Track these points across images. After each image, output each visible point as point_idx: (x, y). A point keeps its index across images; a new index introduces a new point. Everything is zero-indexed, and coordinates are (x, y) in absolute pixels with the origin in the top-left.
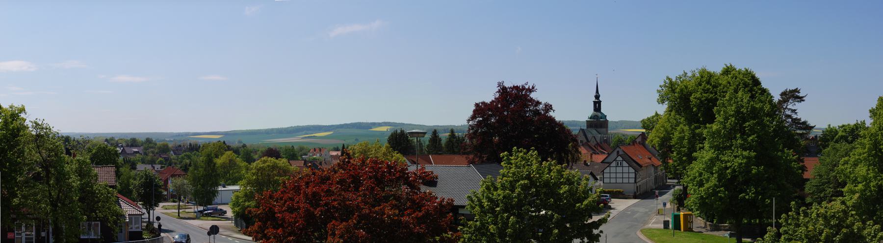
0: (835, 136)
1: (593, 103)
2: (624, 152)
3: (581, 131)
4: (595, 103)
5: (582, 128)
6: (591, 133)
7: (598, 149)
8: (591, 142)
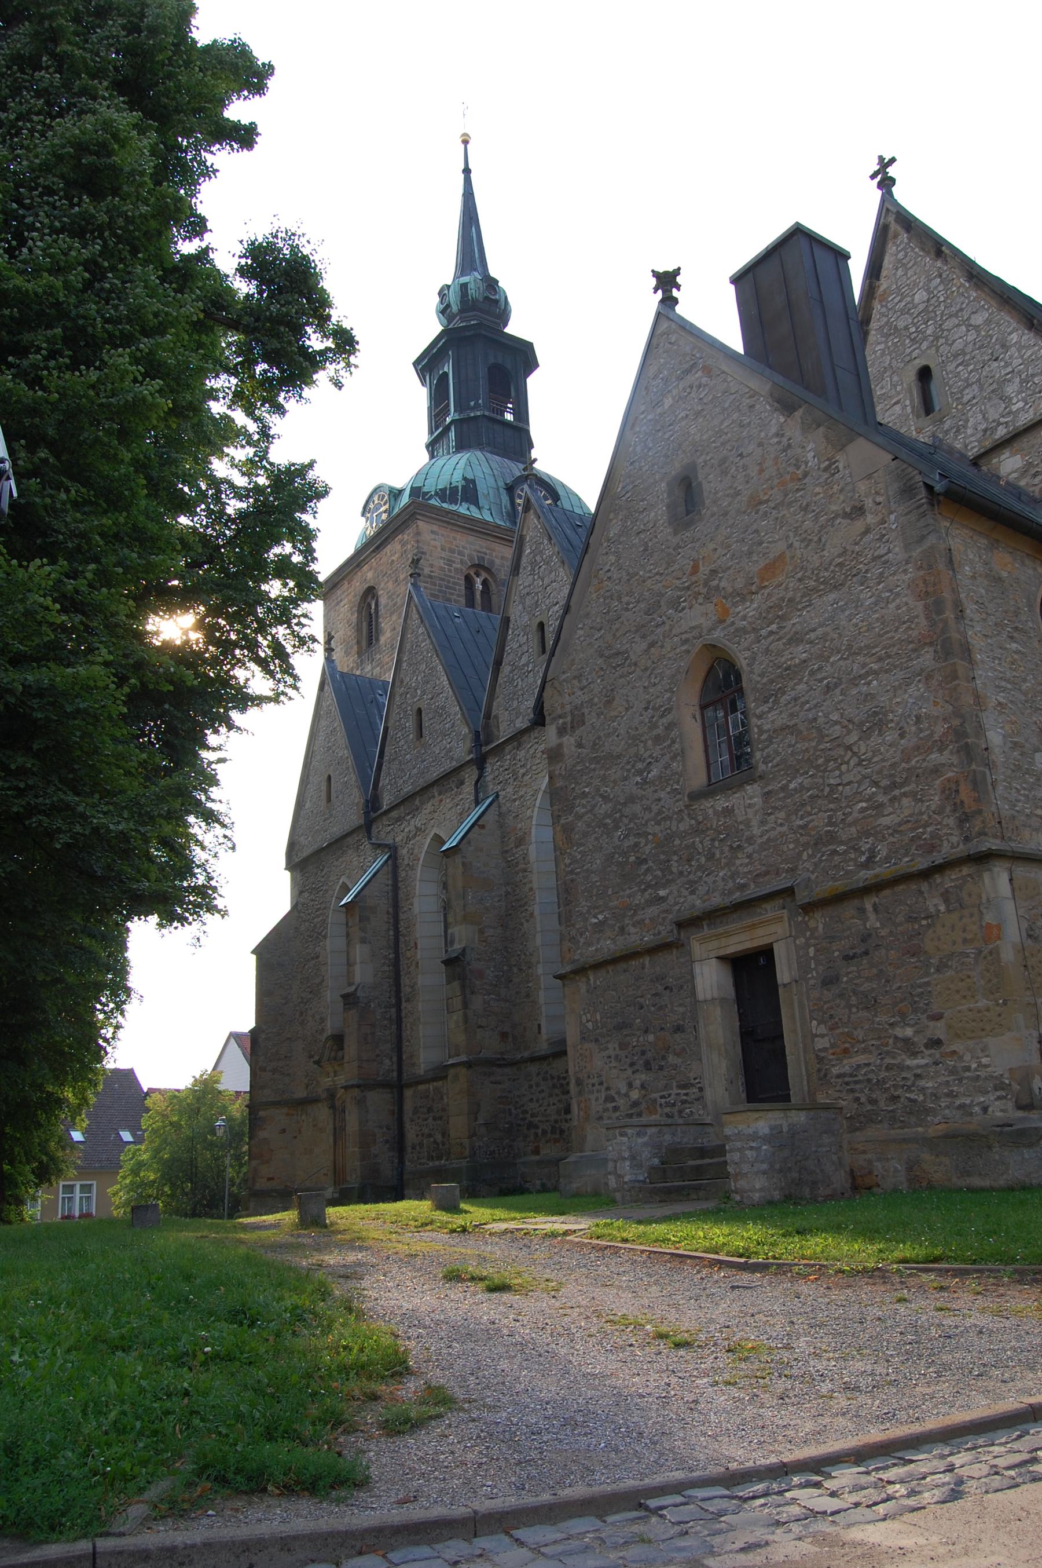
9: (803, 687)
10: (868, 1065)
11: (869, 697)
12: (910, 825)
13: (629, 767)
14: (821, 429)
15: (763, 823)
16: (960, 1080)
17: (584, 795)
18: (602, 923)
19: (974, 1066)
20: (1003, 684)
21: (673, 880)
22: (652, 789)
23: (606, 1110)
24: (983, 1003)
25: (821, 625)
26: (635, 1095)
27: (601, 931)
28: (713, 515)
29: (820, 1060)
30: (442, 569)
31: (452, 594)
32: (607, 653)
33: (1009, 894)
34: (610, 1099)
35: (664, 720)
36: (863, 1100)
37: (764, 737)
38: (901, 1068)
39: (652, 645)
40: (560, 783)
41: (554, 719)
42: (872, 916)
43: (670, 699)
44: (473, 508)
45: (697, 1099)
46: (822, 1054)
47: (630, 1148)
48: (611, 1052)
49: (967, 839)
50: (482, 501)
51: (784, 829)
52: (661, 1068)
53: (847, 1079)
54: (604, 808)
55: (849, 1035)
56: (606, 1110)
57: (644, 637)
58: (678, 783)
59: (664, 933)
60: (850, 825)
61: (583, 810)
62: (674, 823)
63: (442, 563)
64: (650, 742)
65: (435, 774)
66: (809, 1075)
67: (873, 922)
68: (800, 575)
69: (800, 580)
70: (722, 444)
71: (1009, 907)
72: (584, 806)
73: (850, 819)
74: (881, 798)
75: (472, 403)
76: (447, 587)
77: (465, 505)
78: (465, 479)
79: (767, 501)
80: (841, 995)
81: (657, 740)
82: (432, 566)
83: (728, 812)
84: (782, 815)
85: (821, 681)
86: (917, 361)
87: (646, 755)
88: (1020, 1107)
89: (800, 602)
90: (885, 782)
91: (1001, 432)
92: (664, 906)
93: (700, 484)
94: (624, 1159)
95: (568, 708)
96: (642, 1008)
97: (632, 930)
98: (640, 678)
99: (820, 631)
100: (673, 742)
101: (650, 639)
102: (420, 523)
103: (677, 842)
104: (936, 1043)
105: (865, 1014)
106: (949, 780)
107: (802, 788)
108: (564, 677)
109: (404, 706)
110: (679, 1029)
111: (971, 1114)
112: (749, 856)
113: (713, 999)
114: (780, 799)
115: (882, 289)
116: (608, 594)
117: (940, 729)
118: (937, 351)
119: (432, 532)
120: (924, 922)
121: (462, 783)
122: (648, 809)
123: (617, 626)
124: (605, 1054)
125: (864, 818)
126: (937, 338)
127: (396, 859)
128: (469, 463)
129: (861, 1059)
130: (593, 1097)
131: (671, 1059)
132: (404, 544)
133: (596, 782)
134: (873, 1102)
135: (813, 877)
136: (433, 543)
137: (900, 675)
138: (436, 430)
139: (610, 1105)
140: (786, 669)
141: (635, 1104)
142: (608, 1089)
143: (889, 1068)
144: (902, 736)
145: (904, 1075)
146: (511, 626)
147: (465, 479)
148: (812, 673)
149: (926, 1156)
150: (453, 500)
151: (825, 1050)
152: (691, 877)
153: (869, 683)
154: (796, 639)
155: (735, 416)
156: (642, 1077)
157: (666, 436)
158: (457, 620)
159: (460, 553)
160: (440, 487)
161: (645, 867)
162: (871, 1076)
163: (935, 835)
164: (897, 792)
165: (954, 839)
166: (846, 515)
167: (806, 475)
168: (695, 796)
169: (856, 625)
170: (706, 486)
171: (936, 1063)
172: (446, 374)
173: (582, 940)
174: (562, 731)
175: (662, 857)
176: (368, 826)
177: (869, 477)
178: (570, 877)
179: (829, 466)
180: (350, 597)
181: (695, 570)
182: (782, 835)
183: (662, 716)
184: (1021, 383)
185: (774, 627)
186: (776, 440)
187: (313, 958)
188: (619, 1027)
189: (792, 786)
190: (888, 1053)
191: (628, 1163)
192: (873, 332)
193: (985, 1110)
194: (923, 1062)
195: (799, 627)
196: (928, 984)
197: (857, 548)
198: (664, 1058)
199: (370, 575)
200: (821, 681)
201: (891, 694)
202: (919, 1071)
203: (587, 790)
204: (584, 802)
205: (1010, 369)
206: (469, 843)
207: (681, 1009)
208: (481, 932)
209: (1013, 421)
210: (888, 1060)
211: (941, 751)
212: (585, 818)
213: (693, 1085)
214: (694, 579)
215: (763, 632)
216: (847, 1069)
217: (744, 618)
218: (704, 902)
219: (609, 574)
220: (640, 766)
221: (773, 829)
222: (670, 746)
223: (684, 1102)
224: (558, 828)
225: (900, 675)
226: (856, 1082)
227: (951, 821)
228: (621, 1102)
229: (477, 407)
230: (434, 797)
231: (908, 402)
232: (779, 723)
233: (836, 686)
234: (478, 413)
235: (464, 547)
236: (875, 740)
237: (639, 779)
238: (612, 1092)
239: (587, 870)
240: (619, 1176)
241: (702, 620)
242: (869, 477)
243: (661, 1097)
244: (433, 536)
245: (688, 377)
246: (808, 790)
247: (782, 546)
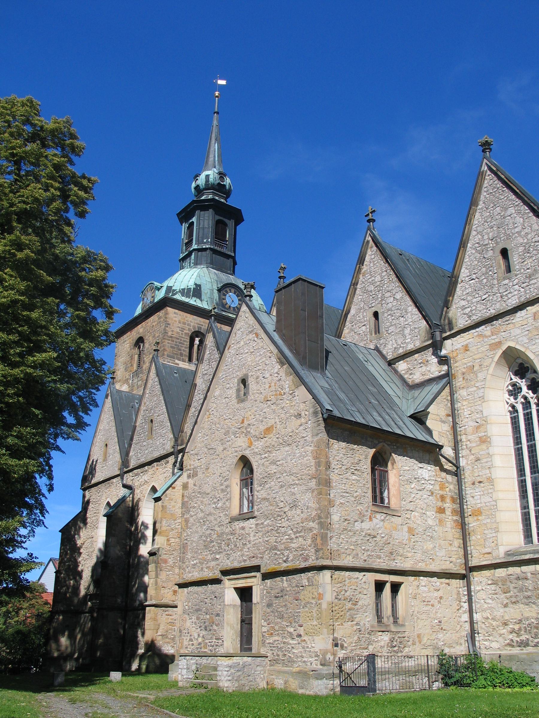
9: (273, 483)
10: (278, 640)
11: (294, 494)
12: (300, 549)
13: (211, 499)
14: (291, 376)
15: (255, 536)
16: (305, 651)
17: (194, 507)
18: (195, 565)
19: (310, 646)
20: (345, 494)
21: (221, 552)
22: (219, 511)
23: (189, 645)
24: (315, 623)
25: (282, 460)
26: (200, 640)
27: (194, 568)
28: (251, 400)
29: (263, 636)
30: (178, 333)
31: (182, 347)
32: (208, 447)
33: (330, 582)
34: (191, 640)
35: (225, 483)
36: (275, 654)
37: (258, 500)
38: (288, 644)
39: (225, 449)
40: (186, 499)
41: (187, 470)
42: (285, 582)
43: (228, 475)
44: (198, 300)
45: (221, 645)
46: (264, 634)
47: (187, 665)
48: (193, 620)
49: (317, 559)
50: (203, 297)
51: (261, 540)
52: (210, 630)
53: (271, 645)
54: (201, 515)
55: (273, 627)
56: (189, 645)
57: (222, 444)
58: (227, 511)
59: (216, 574)
60: (282, 544)
61: (193, 514)
62: (225, 528)
63: (178, 330)
64: (220, 491)
65: (156, 455)
66: (259, 641)
67: (285, 584)
68: (277, 436)
69: (277, 438)
70: (259, 370)
71: (329, 588)
72: (194, 512)
73: (282, 542)
74: (293, 536)
75: (205, 241)
76: (180, 343)
77: (194, 299)
78: (196, 284)
79: (270, 400)
80: (272, 612)
81: (222, 490)
82: (173, 331)
83: (243, 528)
84: (261, 534)
85: (279, 482)
86: (373, 308)
87: (218, 496)
88: (321, 665)
89: (276, 447)
90: (295, 530)
91: (401, 351)
92: (217, 562)
93: (249, 384)
94: (184, 669)
95: (192, 467)
96: (206, 603)
97: (206, 570)
98: (219, 462)
99: (281, 462)
100: (228, 493)
101: (225, 446)
102: (169, 309)
103: (225, 536)
104: (300, 636)
105: (279, 620)
106: (314, 534)
107: (268, 525)
108: (192, 452)
109: (145, 416)
110: (218, 615)
111: (307, 665)
112: (248, 549)
113: (231, 605)
114: (261, 528)
115: (363, 270)
116: (211, 421)
117: (314, 513)
118: (382, 306)
119: (175, 313)
120: (301, 588)
121: (168, 462)
122: (216, 519)
123: (213, 436)
124: (191, 620)
125: (287, 542)
126: (382, 300)
127: (134, 495)
128: (199, 276)
129: (276, 638)
130: (185, 638)
131: (215, 627)
132: (160, 318)
133: (199, 503)
134: (278, 655)
135: (268, 562)
136: (174, 319)
137: (305, 488)
138: (185, 252)
139: (191, 643)
140: (269, 474)
141: (200, 644)
142: (191, 636)
143: (284, 643)
144: (302, 513)
145: (289, 646)
146: (197, 388)
147: (196, 284)
148: (277, 479)
149: (291, 679)
150: (188, 296)
151: (265, 632)
152: (228, 552)
153: (294, 488)
154: (274, 463)
155: (264, 359)
156: (204, 633)
157: (240, 358)
158: (175, 375)
159: (189, 325)
160: (189, 269)
161: (213, 544)
162: (278, 645)
163: (307, 555)
164: (298, 535)
165: (313, 558)
166: (295, 416)
167: (284, 394)
168: (233, 520)
169: (293, 463)
170: (250, 386)
171: (299, 644)
172: (193, 222)
173: (187, 570)
174: (189, 477)
175: (219, 541)
176: (121, 476)
177: (304, 402)
178: (185, 541)
179: (292, 393)
180: (131, 340)
181: (243, 422)
182: (260, 542)
183: (225, 481)
184: (411, 330)
185: (266, 455)
186: (276, 375)
187: (90, 538)
188: (197, 610)
189: (265, 523)
190: (285, 637)
191: (185, 670)
192: (358, 289)
193: (311, 664)
194: (295, 642)
195: (274, 458)
196: (299, 612)
197: (297, 431)
198: (212, 626)
199: (141, 330)
200: (279, 482)
201: (300, 495)
202: (293, 646)
203: (195, 505)
204: (194, 510)
205: (407, 323)
206: (166, 496)
207: (220, 607)
208: (168, 540)
209: (406, 347)
210: (284, 640)
211: (313, 522)
212: (194, 517)
213: (221, 639)
214: (242, 425)
215: (263, 456)
216: (271, 641)
217: (257, 448)
218: (231, 564)
219: (213, 412)
220: (215, 500)
221: (257, 539)
222: (226, 495)
223: (217, 645)
224: (183, 519)
225: (305, 488)
226: (274, 647)
227: (313, 550)
228: (195, 642)
229: (207, 242)
230: (154, 466)
231: (368, 327)
232: (264, 496)
233: (284, 486)
234: (207, 246)
235: (191, 322)
236: (294, 512)
237: (214, 506)
238: (192, 637)
239: (192, 540)
240: (182, 675)
241: (243, 444)
242: (304, 402)
243: (210, 642)
244: (175, 315)
245: (250, 335)
246: (271, 526)
247: (273, 421)
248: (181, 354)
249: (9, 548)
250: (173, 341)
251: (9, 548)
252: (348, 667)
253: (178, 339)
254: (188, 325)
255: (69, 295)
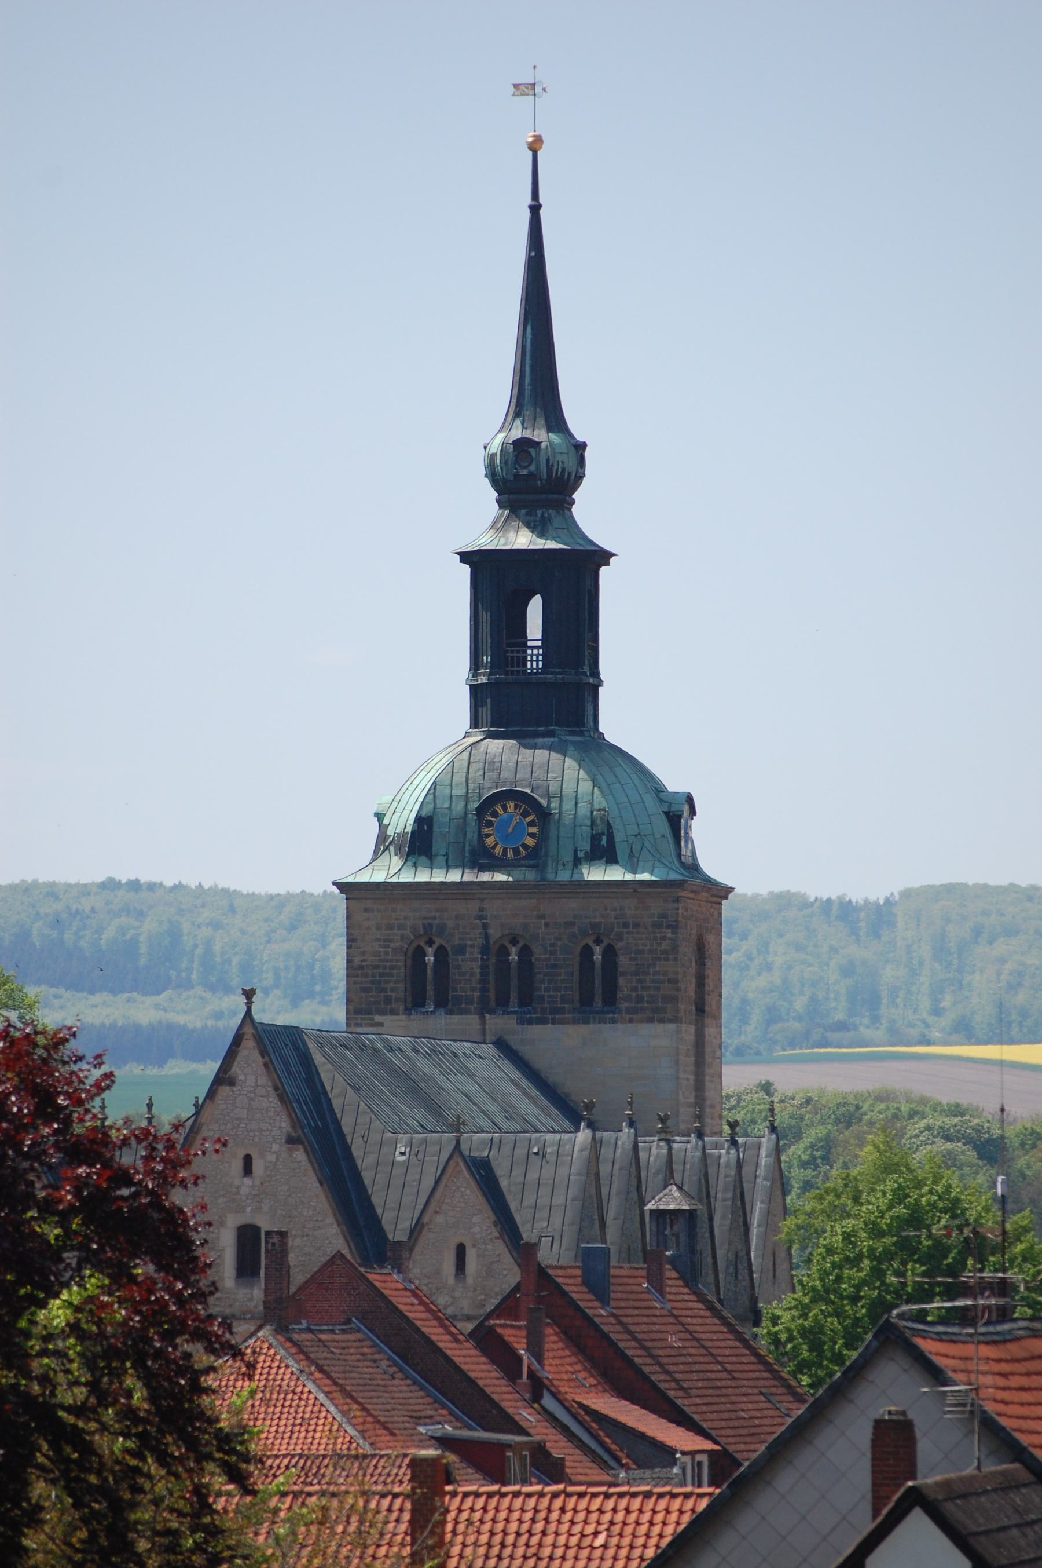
0: (346, 1258)
1: (528, 210)
2: (989, 1427)
3: (250, 1060)
4: (531, 207)
5: (269, 1014)
6: (434, 1108)
7: (537, 1388)
8: (419, 1265)
31: (387, 982)
248: (388, 1000)
249: (301, 1323)
250: (366, 975)
251: (301, 1323)
252: (226, 1165)
253: (378, 967)
254: (399, 929)
255: (199, 1480)
